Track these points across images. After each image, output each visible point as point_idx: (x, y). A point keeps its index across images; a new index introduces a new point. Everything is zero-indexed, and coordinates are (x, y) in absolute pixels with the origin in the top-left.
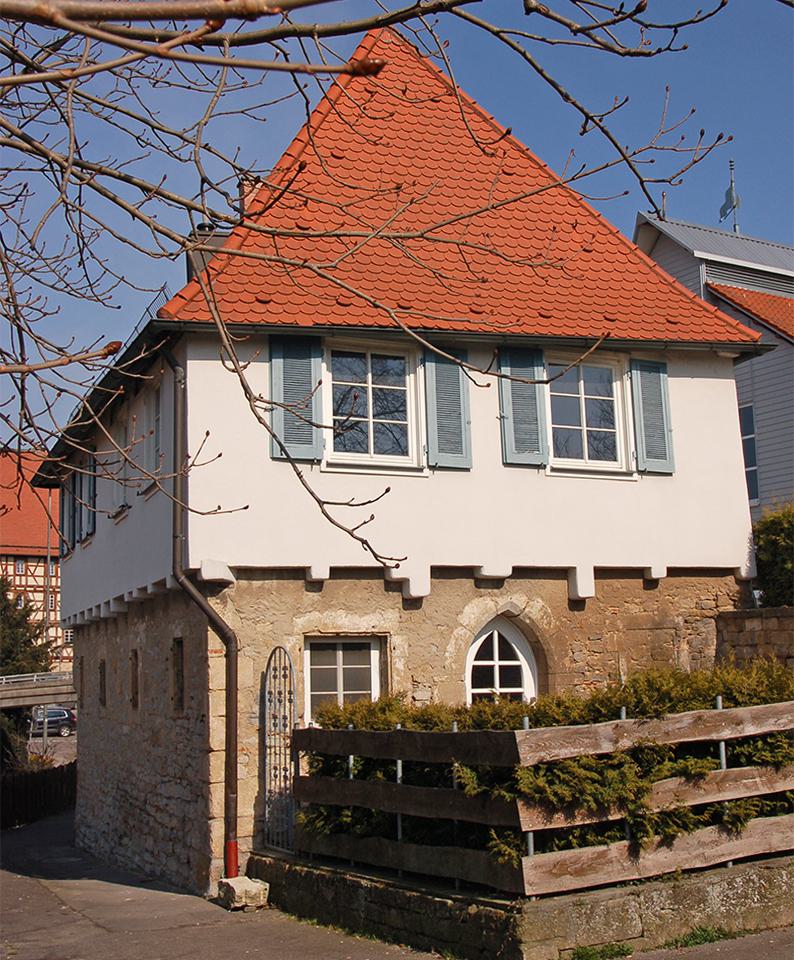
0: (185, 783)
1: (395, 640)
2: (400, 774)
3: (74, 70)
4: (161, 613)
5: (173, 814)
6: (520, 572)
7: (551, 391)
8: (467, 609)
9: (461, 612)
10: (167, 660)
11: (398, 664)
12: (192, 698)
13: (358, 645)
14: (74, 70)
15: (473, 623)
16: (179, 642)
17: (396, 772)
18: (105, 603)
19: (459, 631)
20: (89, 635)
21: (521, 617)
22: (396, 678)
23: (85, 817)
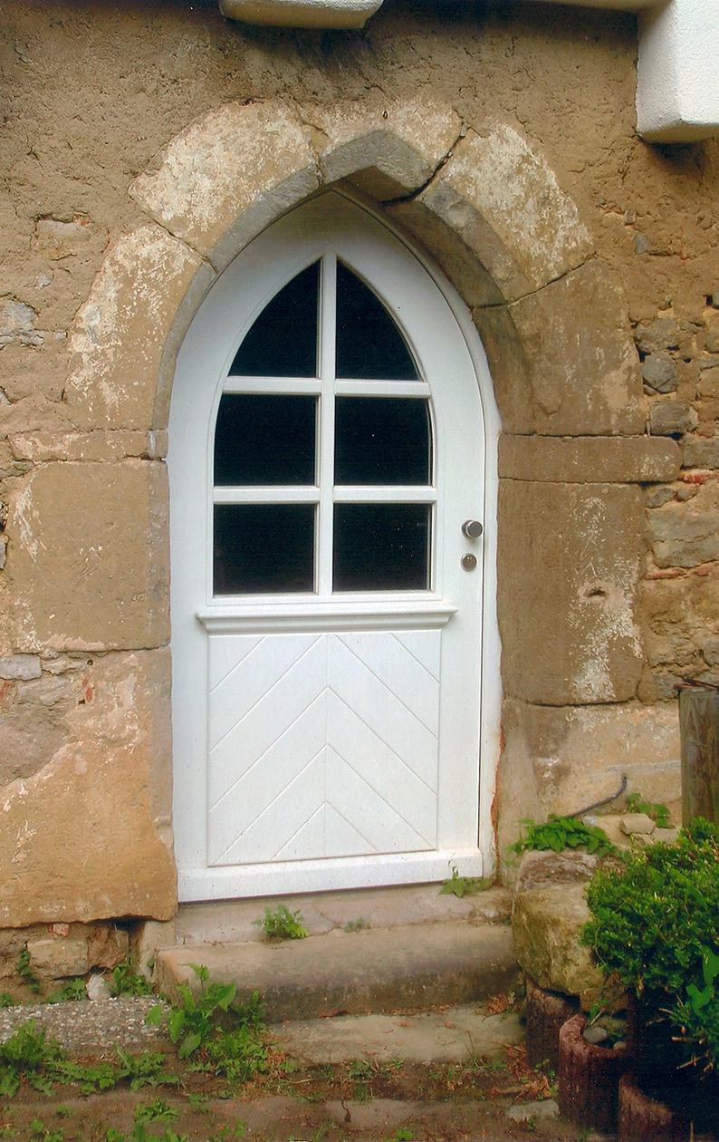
8: (182, 154)
9: (151, 165)
15: (206, 212)
19: (137, 246)
21: (428, 197)
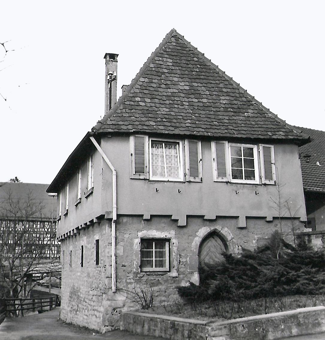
0: (98, 289)
1: (173, 241)
2: (144, 250)
3: (263, 177)
4: (92, 233)
5: (94, 301)
6: (218, 217)
7: (231, 156)
10: (93, 248)
11: (174, 249)
12: (102, 260)
13: (161, 242)
14: (263, 177)
16: (97, 241)
17: (144, 249)
18: (72, 230)
20: (66, 243)
21: (219, 233)
22: (174, 254)
23: (64, 307)
